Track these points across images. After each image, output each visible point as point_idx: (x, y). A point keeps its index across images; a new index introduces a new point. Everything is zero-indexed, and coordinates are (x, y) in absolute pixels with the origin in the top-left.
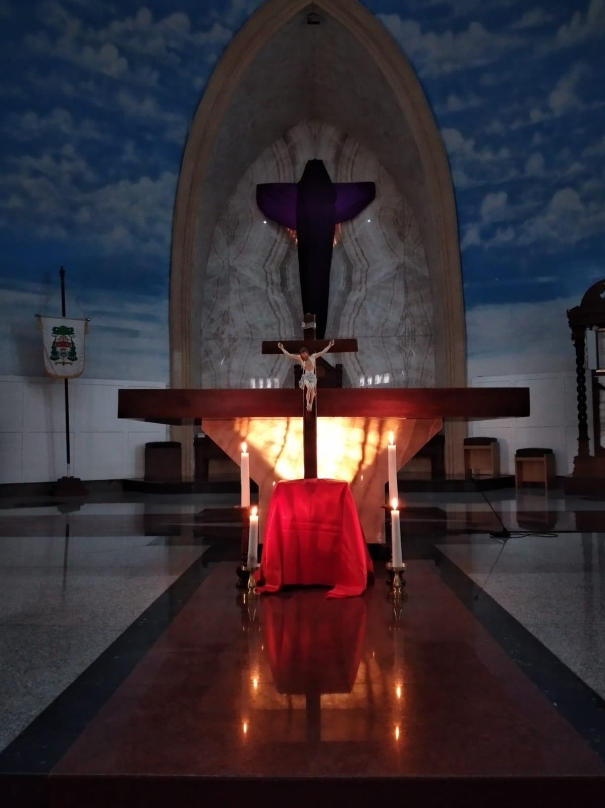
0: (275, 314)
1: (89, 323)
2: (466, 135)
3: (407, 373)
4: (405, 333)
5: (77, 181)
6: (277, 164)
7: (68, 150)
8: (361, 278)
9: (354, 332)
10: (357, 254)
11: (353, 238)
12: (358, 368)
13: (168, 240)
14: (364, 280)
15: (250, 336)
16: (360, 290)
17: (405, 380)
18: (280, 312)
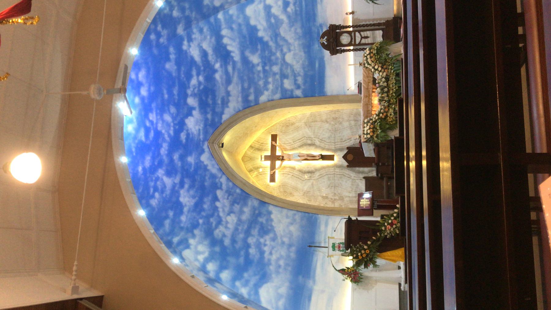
0: (324, 176)
1: (330, 237)
2: (262, 94)
3: (351, 120)
4: (333, 122)
6: (260, 175)
7: (262, 240)
8: (310, 140)
9: (332, 143)
10: (300, 142)
11: (293, 143)
12: (349, 140)
13: (295, 212)
14: (310, 139)
15: (333, 187)
16: (315, 140)
17: (354, 121)
18: (323, 174)
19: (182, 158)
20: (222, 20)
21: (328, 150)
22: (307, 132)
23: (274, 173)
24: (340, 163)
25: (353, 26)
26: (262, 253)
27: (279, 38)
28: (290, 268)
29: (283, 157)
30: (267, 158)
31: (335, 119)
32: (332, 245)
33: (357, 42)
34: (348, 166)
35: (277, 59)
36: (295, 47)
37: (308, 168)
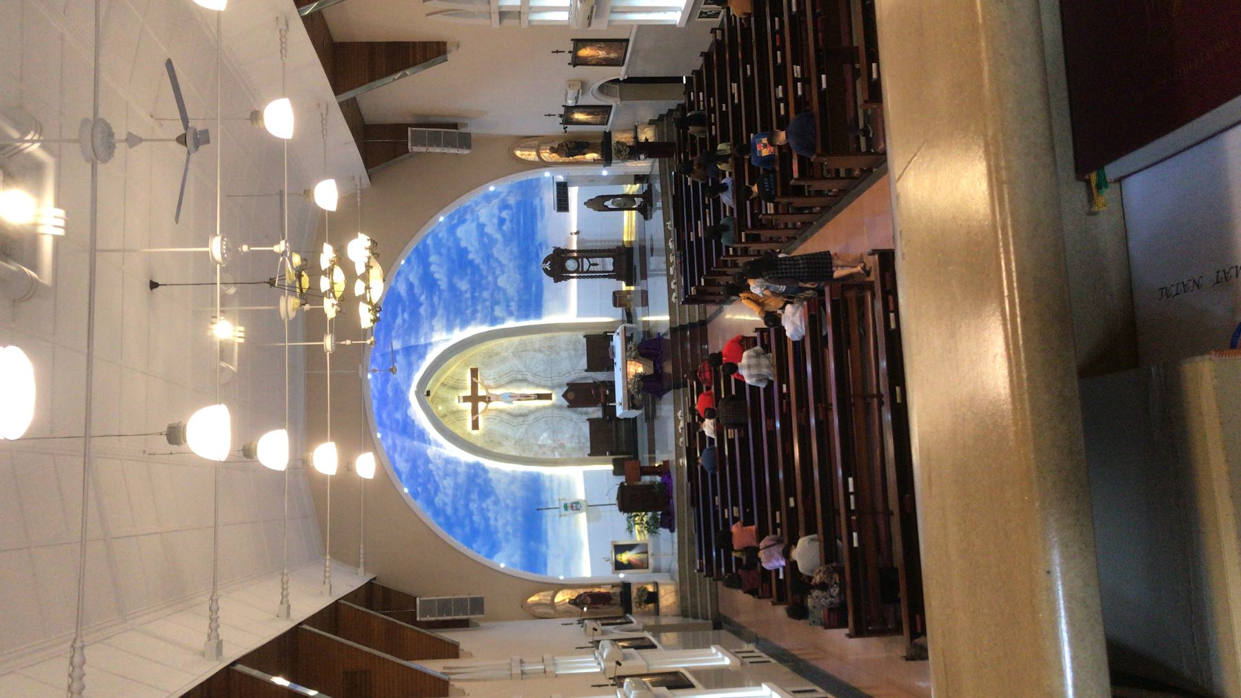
5: (496, 503)
7: (484, 505)
16: (527, 375)
19: (390, 415)
20: (431, 245)
21: (544, 387)
22: (517, 364)
23: (477, 418)
24: (559, 403)
25: (578, 251)
26: (487, 519)
27: (491, 260)
28: (519, 534)
29: (489, 398)
30: (466, 399)
31: (550, 348)
32: (563, 506)
33: (585, 269)
34: (568, 407)
35: (488, 283)
36: (509, 269)
37: (519, 409)
